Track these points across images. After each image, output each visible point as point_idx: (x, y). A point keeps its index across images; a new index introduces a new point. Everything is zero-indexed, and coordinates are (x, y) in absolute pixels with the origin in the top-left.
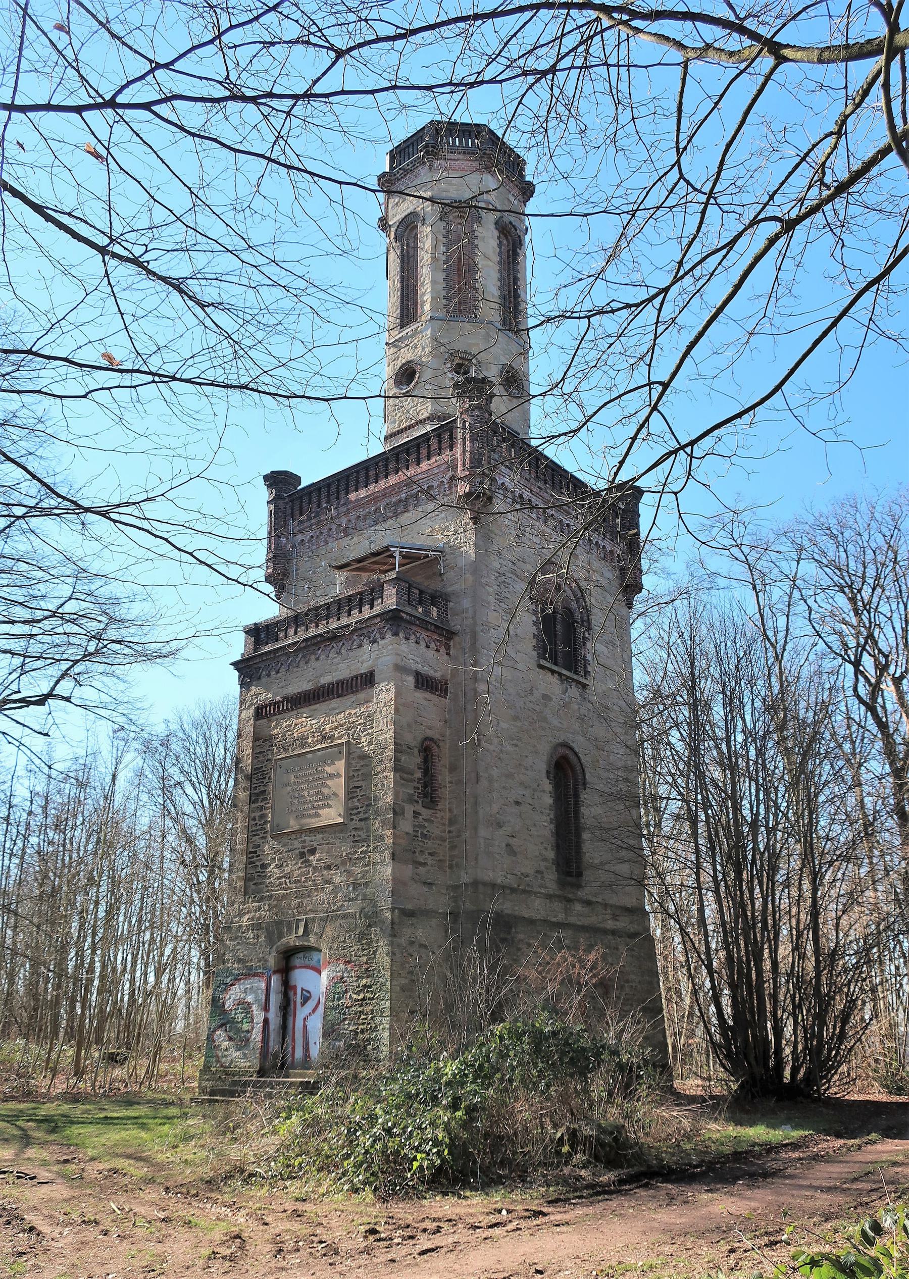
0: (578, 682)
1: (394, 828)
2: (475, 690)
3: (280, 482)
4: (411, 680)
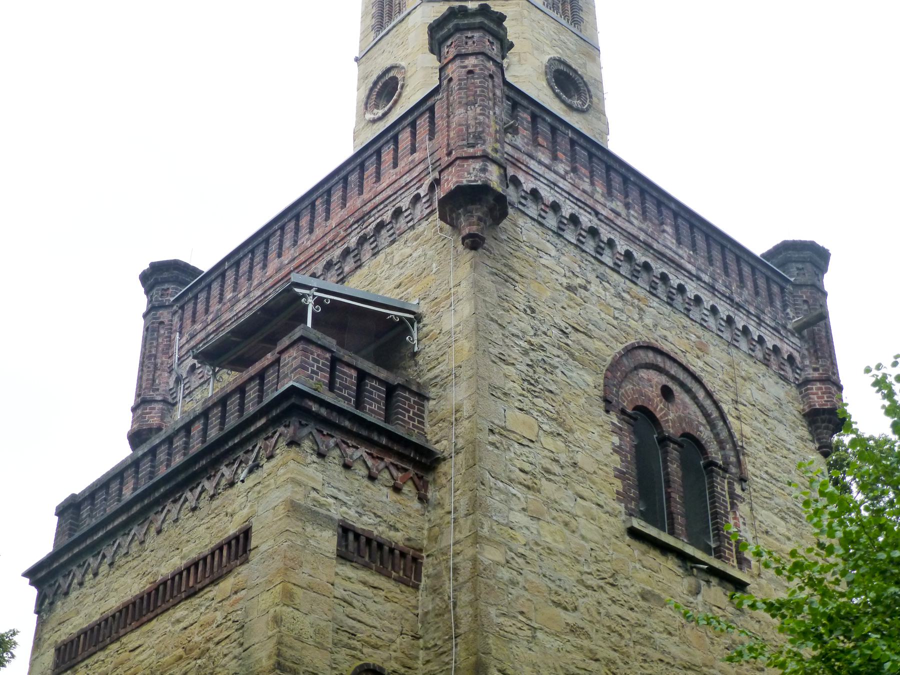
0: (724, 578)
2: (475, 560)
4: (328, 540)
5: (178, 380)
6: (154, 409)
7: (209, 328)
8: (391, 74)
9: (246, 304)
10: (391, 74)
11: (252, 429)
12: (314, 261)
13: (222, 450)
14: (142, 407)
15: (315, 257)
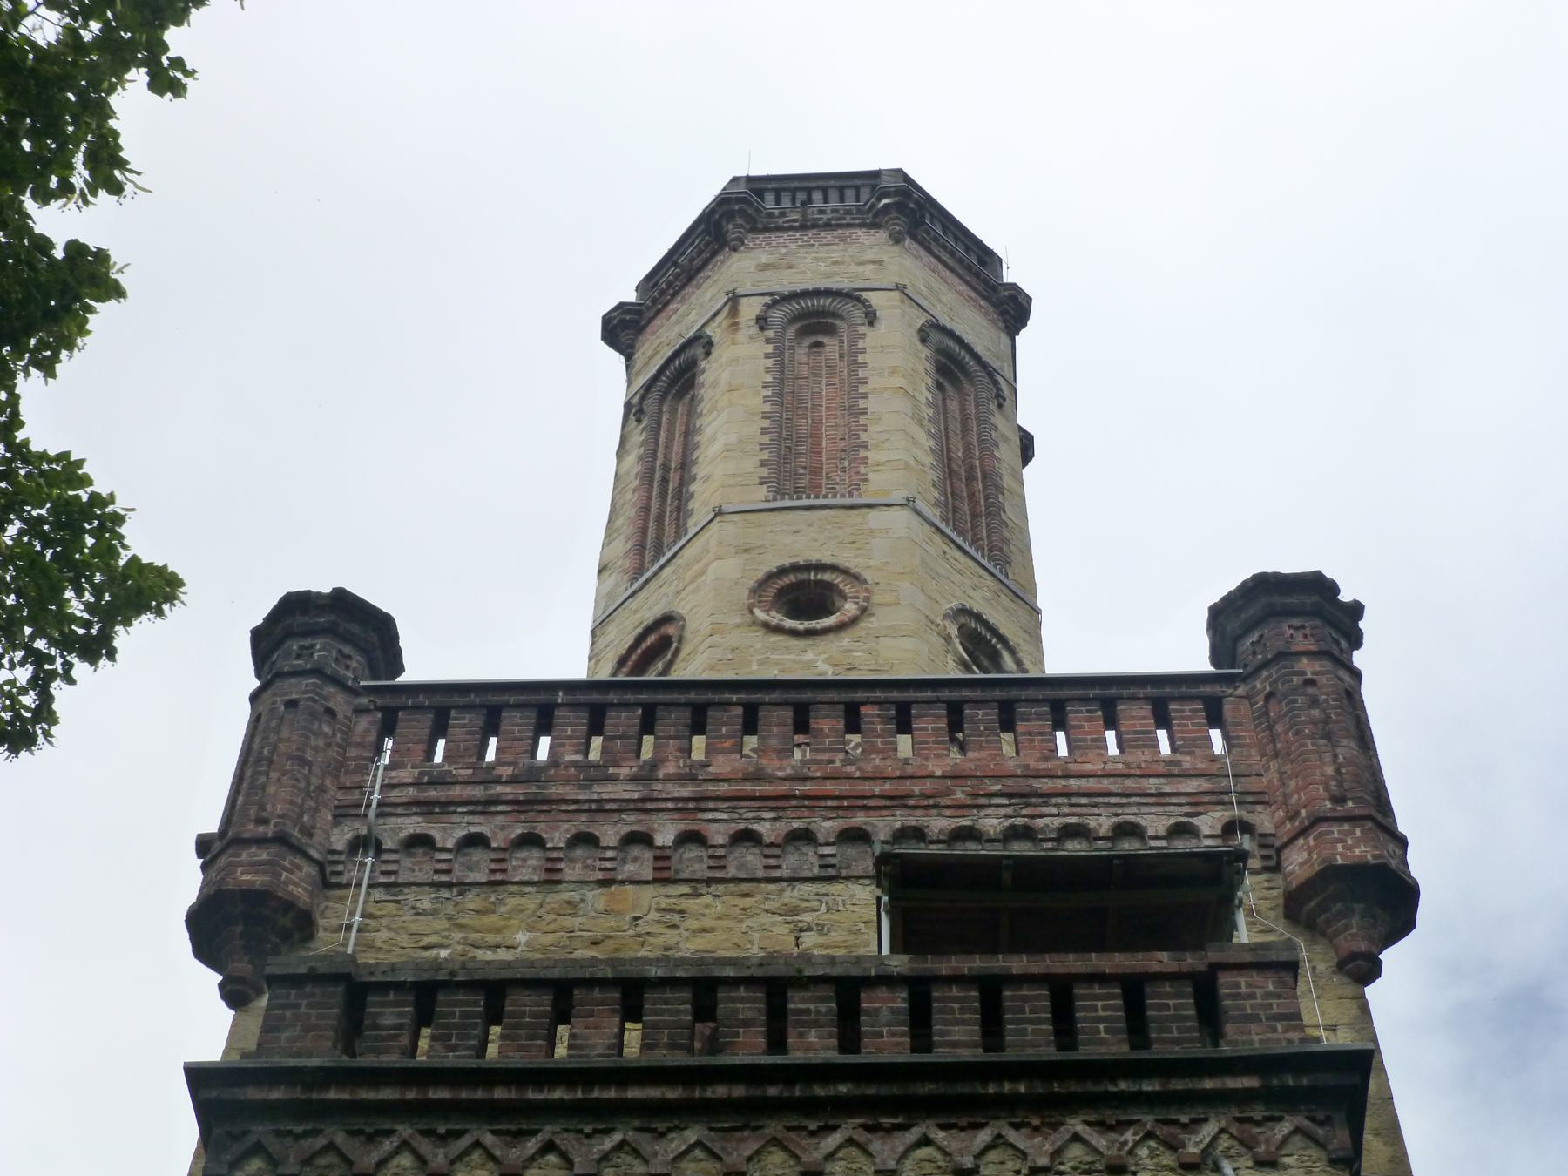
5: (360, 844)
6: (300, 869)
7: (499, 789)
9: (636, 796)
10: (827, 576)
11: (1208, 1084)
12: (865, 808)
13: (1100, 1088)
14: (274, 849)
15: (871, 803)
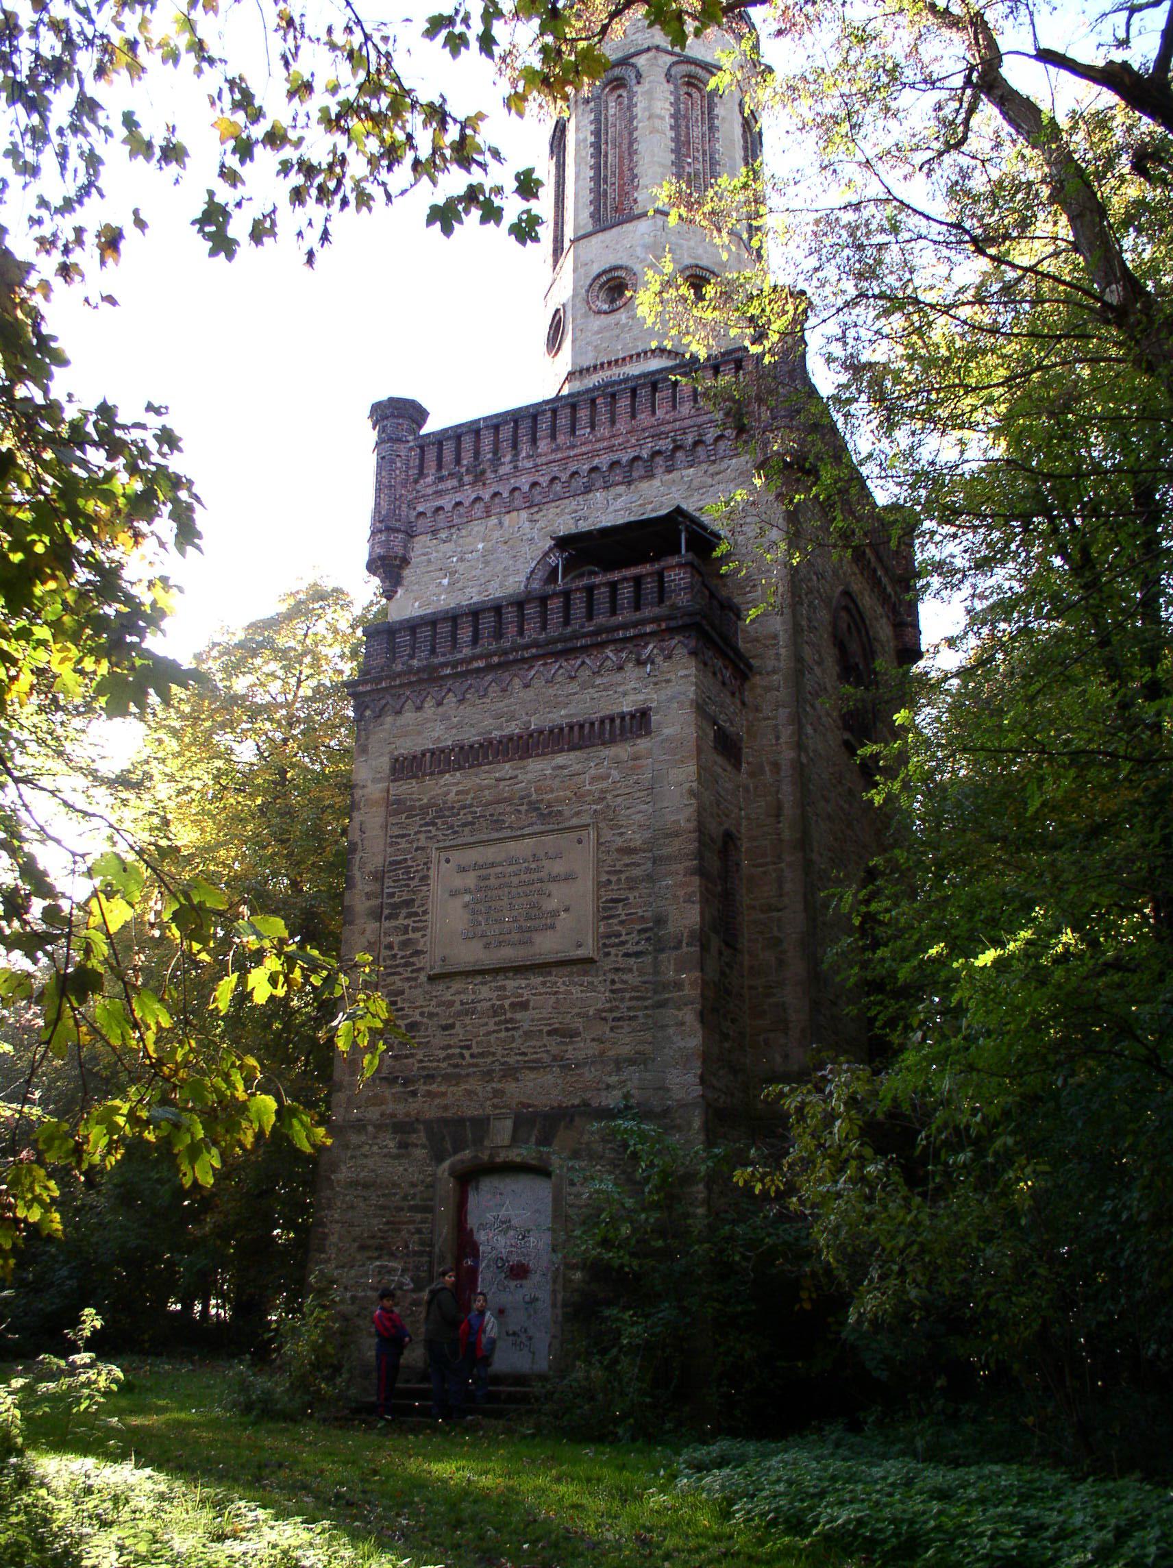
1: (702, 970)
3: (397, 418)
8: (622, 273)
